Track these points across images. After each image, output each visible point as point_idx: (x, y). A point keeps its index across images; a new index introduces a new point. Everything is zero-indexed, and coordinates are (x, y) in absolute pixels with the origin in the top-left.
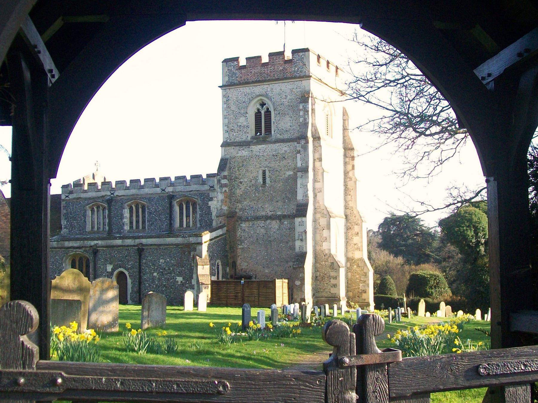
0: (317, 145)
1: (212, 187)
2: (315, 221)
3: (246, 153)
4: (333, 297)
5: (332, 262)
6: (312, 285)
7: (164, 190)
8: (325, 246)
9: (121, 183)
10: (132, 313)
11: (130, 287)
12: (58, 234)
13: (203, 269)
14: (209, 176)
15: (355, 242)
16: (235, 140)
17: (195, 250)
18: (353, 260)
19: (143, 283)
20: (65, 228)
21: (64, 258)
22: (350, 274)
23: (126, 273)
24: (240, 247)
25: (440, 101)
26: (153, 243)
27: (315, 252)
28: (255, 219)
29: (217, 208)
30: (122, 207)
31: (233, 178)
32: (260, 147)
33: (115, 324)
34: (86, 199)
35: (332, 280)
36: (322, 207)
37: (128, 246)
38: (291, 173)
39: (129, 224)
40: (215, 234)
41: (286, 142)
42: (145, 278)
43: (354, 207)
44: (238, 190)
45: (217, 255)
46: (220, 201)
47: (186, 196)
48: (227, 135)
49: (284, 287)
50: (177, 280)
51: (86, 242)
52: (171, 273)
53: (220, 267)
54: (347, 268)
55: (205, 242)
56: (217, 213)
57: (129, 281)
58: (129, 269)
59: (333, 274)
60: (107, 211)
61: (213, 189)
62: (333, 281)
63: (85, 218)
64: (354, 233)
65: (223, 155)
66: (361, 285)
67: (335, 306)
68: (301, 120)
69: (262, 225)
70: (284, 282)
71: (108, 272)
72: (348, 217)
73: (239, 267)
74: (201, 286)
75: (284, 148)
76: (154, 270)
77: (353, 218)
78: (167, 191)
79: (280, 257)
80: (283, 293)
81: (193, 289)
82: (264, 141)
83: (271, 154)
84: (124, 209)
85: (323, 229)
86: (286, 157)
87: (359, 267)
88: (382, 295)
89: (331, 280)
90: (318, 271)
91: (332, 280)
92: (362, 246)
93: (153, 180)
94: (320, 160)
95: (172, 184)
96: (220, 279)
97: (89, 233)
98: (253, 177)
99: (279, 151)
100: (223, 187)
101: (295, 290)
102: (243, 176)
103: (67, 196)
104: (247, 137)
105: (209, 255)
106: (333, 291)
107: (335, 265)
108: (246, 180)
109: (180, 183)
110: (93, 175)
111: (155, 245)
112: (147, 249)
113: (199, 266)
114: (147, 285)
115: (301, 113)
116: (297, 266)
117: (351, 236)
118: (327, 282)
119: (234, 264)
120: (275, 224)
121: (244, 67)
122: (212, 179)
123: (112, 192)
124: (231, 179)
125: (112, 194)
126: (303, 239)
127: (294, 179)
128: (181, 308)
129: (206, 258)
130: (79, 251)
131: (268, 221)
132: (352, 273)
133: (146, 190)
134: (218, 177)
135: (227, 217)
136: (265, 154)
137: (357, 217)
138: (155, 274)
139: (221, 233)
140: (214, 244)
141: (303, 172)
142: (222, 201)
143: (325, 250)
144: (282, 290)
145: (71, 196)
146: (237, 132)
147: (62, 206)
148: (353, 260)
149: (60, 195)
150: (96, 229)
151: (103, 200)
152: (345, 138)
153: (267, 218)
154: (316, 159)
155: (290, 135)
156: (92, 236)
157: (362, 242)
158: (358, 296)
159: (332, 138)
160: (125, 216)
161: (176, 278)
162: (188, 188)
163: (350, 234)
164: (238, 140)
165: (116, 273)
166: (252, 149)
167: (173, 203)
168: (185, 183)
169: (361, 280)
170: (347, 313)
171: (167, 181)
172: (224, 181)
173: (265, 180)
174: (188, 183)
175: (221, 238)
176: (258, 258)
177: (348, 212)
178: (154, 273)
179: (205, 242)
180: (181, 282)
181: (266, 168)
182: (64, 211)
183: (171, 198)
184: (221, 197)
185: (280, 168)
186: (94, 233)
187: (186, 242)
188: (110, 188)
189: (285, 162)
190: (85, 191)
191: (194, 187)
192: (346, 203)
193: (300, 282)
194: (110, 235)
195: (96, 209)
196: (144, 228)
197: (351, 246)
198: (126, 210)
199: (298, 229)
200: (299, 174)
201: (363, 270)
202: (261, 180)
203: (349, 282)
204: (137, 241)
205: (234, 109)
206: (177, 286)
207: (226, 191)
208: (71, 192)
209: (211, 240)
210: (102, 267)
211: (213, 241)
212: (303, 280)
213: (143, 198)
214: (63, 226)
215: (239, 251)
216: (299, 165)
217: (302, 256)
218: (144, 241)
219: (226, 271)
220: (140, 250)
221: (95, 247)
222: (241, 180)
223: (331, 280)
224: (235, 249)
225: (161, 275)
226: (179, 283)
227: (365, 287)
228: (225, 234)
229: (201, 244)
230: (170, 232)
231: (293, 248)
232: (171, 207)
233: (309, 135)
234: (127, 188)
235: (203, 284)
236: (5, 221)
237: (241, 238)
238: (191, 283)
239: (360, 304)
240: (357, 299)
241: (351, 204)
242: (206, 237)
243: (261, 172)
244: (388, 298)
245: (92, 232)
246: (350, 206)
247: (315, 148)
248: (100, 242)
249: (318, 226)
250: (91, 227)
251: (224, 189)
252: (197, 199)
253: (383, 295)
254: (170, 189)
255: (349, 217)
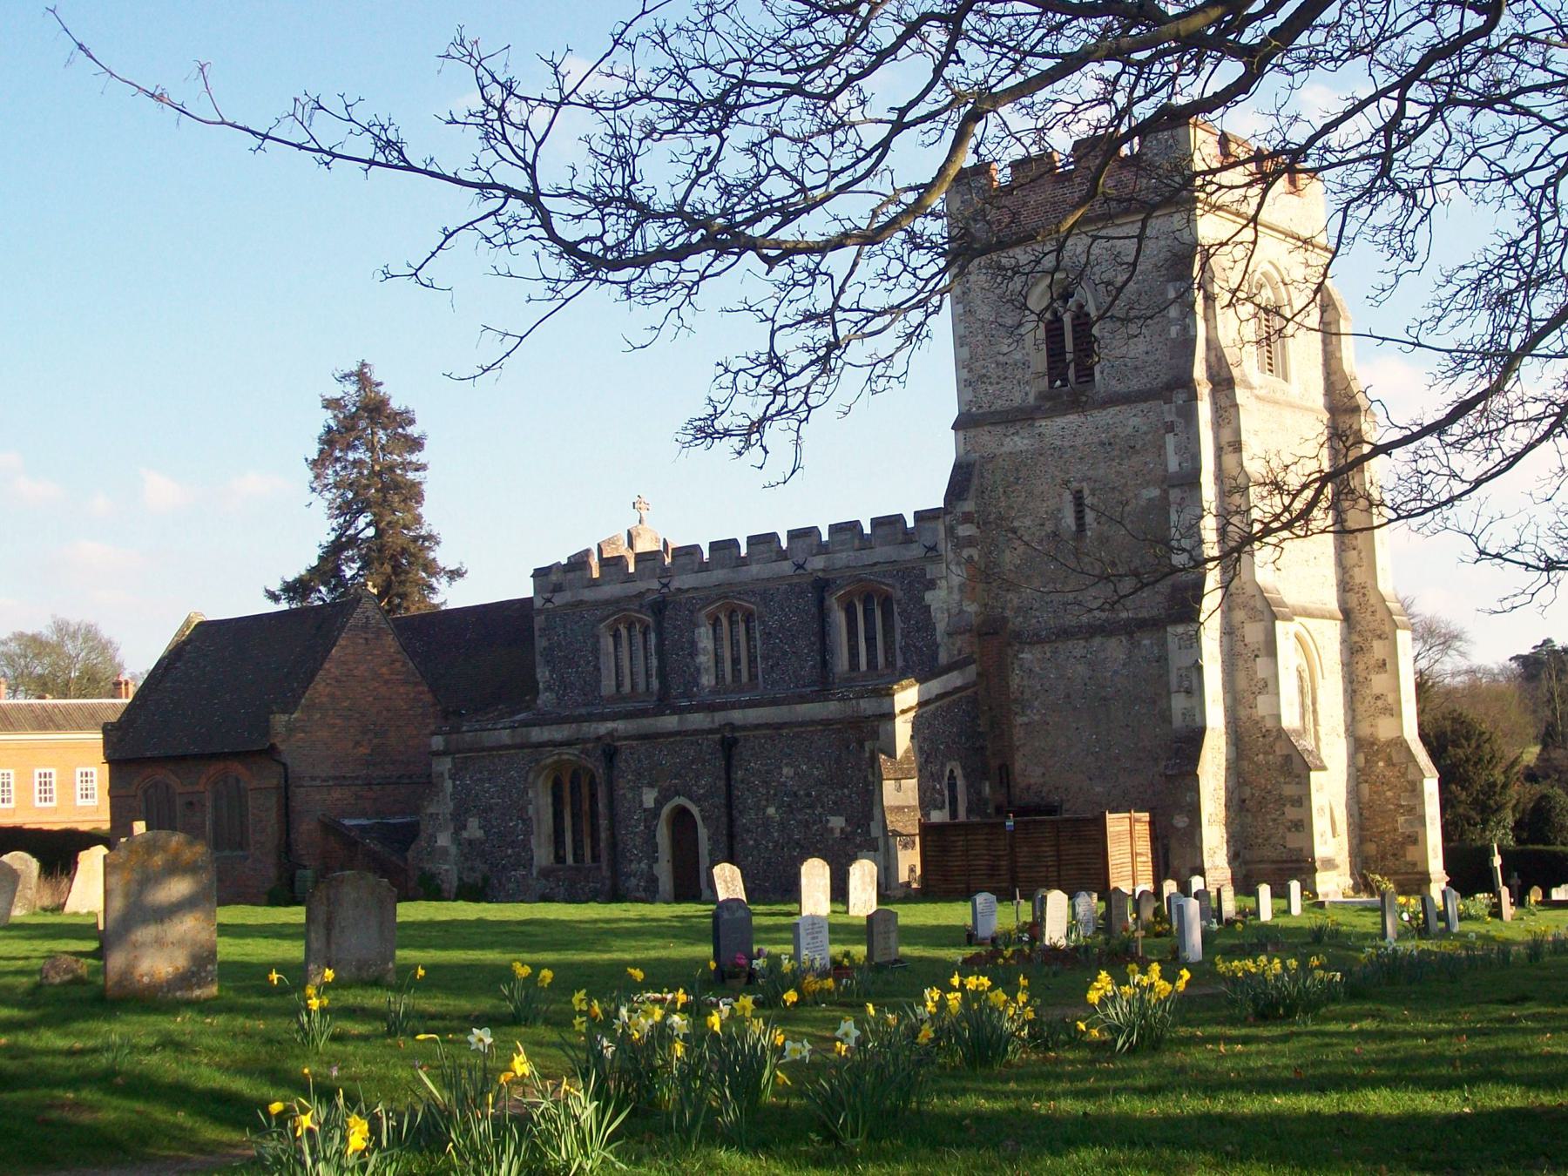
0: (1224, 402)
1: (933, 548)
2: (1229, 632)
3: (1025, 442)
4: (1292, 861)
5: (1285, 752)
6: (1227, 825)
7: (800, 567)
8: (1262, 706)
9: (687, 554)
10: (627, 929)
11: (706, 852)
12: (528, 708)
13: (899, 789)
14: (920, 516)
15: (1377, 690)
16: (993, 408)
17: (875, 735)
18: (1373, 744)
19: (739, 838)
20: (549, 688)
21: (531, 776)
22: (1365, 788)
23: (695, 810)
24: (1020, 720)
25: (720, 136)
26: (760, 721)
27: (1237, 726)
28: (1058, 636)
29: (948, 610)
30: (691, 621)
31: (992, 517)
32: (1061, 421)
33: (203, 974)
34: (596, 604)
35: (1288, 809)
36: (1250, 590)
37: (696, 732)
38: (1155, 492)
39: (713, 670)
40: (936, 686)
41: (1135, 402)
42: (744, 825)
43: (1368, 585)
44: (1008, 552)
45: (948, 746)
46: (956, 590)
47: (861, 580)
48: (969, 395)
49: (1136, 835)
50: (830, 825)
51: (585, 727)
52: (812, 806)
53: (961, 783)
54: (1358, 771)
55: (903, 712)
56: (948, 624)
57: (703, 832)
58: (699, 800)
59: (1290, 790)
60: (653, 636)
61: (935, 553)
62: (1292, 813)
63: (598, 658)
64: (1372, 662)
65: (962, 452)
66: (1401, 819)
67: (1295, 886)
68: (1174, 331)
69: (1078, 652)
70: (1138, 821)
71: (645, 810)
72: (1352, 616)
73: (1019, 780)
74: (891, 840)
75: (1130, 420)
76: (767, 800)
77: (1369, 618)
78: (809, 567)
79: (1136, 744)
80: (1134, 855)
81: (876, 850)
82: (1077, 404)
83: (1096, 440)
84: (699, 626)
85: (1257, 656)
86: (1138, 447)
87: (1394, 765)
88: (1536, 847)
89: (1286, 809)
90: (1246, 783)
91: (1288, 809)
92: (1399, 701)
93: (772, 537)
94: (1237, 447)
95: (823, 548)
96: (962, 816)
97: (611, 700)
98: (1046, 512)
99: (1119, 430)
100: (964, 547)
101: (1174, 844)
102: (1019, 511)
103: (549, 600)
104: (1027, 394)
105: (921, 748)
106: (1294, 841)
107: (1297, 767)
108: (1028, 522)
109: (843, 543)
110: (630, 534)
111: (767, 726)
112: (746, 739)
113: (886, 783)
114: (751, 843)
115: (1173, 312)
116: (1174, 772)
117: (1364, 674)
118: (1274, 816)
119: (1004, 775)
120: (1115, 649)
121: (1007, 190)
122: (927, 525)
123: (664, 581)
124: (985, 523)
125: (665, 585)
126: (1194, 689)
127: (1162, 506)
128: (793, 908)
129: (908, 758)
130: (569, 754)
131: (1097, 641)
132: (1374, 784)
133: (755, 569)
134: (948, 518)
135: (980, 635)
136: (1079, 441)
137: (1378, 616)
138: (771, 811)
139: (959, 683)
140: (934, 715)
141: (1186, 488)
142: (962, 588)
143: (1263, 717)
144: (1132, 845)
145: (559, 599)
146: (998, 383)
147: (536, 628)
148: (1373, 744)
149: (530, 599)
150: (627, 688)
151: (641, 606)
152: (1333, 378)
153: (1091, 631)
154: (1226, 447)
155: (1145, 380)
156: (617, 707)
157: (1397, 689)
158: (1394, 855)
159: (1286, 379)
160: (701, 645)
161: (828, 821)
162: (868, 557)
163: (1361, 666)
164: (999, 404)
165: (666, 810)
166: (1041, 429)
167: (827, 603)
168: (857, 542)
169: (1402, 806)
170: (1315, 910)
171: (808, 540)
172: (965, 530)
173: (1083, 517)
174: (865, 542)
175: (961, 698)
176: (1073, 752)
177: (1353, 600)
178: (766, 807)
179: (903, 712)
180: (842, 830)
181: (1084, 484)
182: (541, 643)
183: (823, 589)
184: (957, 576)
185: (1123, 481)
186: (624, 699)
187: (849, 712)
188: (658, 571)
189: (1136, 461)
190: (594, 583)
191: (882, 553)
192: (1344, 573)
193: (1186, 819)
194: (664, 704)
195: (624, 632)
196: (753, 677)
197: (1366, 704)
198: (703, 630)
199: (1178, 660)
200: (1174, 494)
201: (1404, 775)
202: (1069, 520)
203: (1366, 813)
204: (720, 718)
205: (986, 317)
206: (830, 842)
207: (971, 557)
208: (558, 588)
209: (921, 704)
210: (630, 796)
211: (932, 707)
212: (1194, 811)
213: (746, 593)
214: (541, 685)
215: (1019, 734)
216: (1173, 465)
217: (1195, 737)
218: (737, 716)
219: (979, 793)
220: (729, 744)
221: (609, 741)
222: (1016, 524)
223: (1286, 809)
224: (1005, 727)
225: (785, 812)
226: (837, 833)
227: (1412, 826)
228: (975, 684)
229: (891, 716)
230: (823, 685)
231: (1166, 717)
232: (823, 615)
233: (1199, 371)
234: (704, 567)
235: (896, 834)
236: (387, 677)
237: (1022, 693)
238: (868, 832)
239: (1401, 877)
240: (1390, 862)
241: (1359, 576)
242: (907, 697)
243: (1068, 497)
244: (1555, 854)
245: (618, 697)
246: (1357, 581)
247: (1221, 412)
248: (620, 726)
249: (1239, 647)
250: (614, 683)
251: (965, 553)
252: (893, 587)
253: (1541, 847)
254: (818, 563)
255: (1357, 616)
